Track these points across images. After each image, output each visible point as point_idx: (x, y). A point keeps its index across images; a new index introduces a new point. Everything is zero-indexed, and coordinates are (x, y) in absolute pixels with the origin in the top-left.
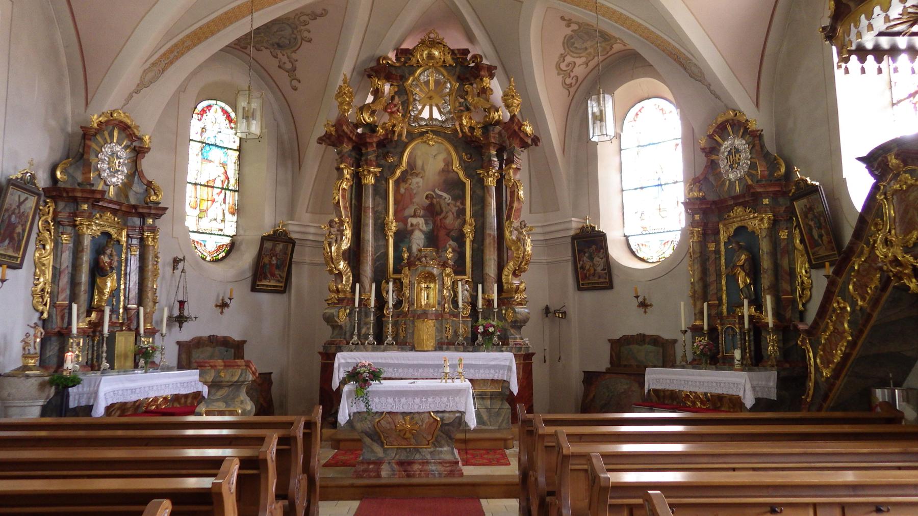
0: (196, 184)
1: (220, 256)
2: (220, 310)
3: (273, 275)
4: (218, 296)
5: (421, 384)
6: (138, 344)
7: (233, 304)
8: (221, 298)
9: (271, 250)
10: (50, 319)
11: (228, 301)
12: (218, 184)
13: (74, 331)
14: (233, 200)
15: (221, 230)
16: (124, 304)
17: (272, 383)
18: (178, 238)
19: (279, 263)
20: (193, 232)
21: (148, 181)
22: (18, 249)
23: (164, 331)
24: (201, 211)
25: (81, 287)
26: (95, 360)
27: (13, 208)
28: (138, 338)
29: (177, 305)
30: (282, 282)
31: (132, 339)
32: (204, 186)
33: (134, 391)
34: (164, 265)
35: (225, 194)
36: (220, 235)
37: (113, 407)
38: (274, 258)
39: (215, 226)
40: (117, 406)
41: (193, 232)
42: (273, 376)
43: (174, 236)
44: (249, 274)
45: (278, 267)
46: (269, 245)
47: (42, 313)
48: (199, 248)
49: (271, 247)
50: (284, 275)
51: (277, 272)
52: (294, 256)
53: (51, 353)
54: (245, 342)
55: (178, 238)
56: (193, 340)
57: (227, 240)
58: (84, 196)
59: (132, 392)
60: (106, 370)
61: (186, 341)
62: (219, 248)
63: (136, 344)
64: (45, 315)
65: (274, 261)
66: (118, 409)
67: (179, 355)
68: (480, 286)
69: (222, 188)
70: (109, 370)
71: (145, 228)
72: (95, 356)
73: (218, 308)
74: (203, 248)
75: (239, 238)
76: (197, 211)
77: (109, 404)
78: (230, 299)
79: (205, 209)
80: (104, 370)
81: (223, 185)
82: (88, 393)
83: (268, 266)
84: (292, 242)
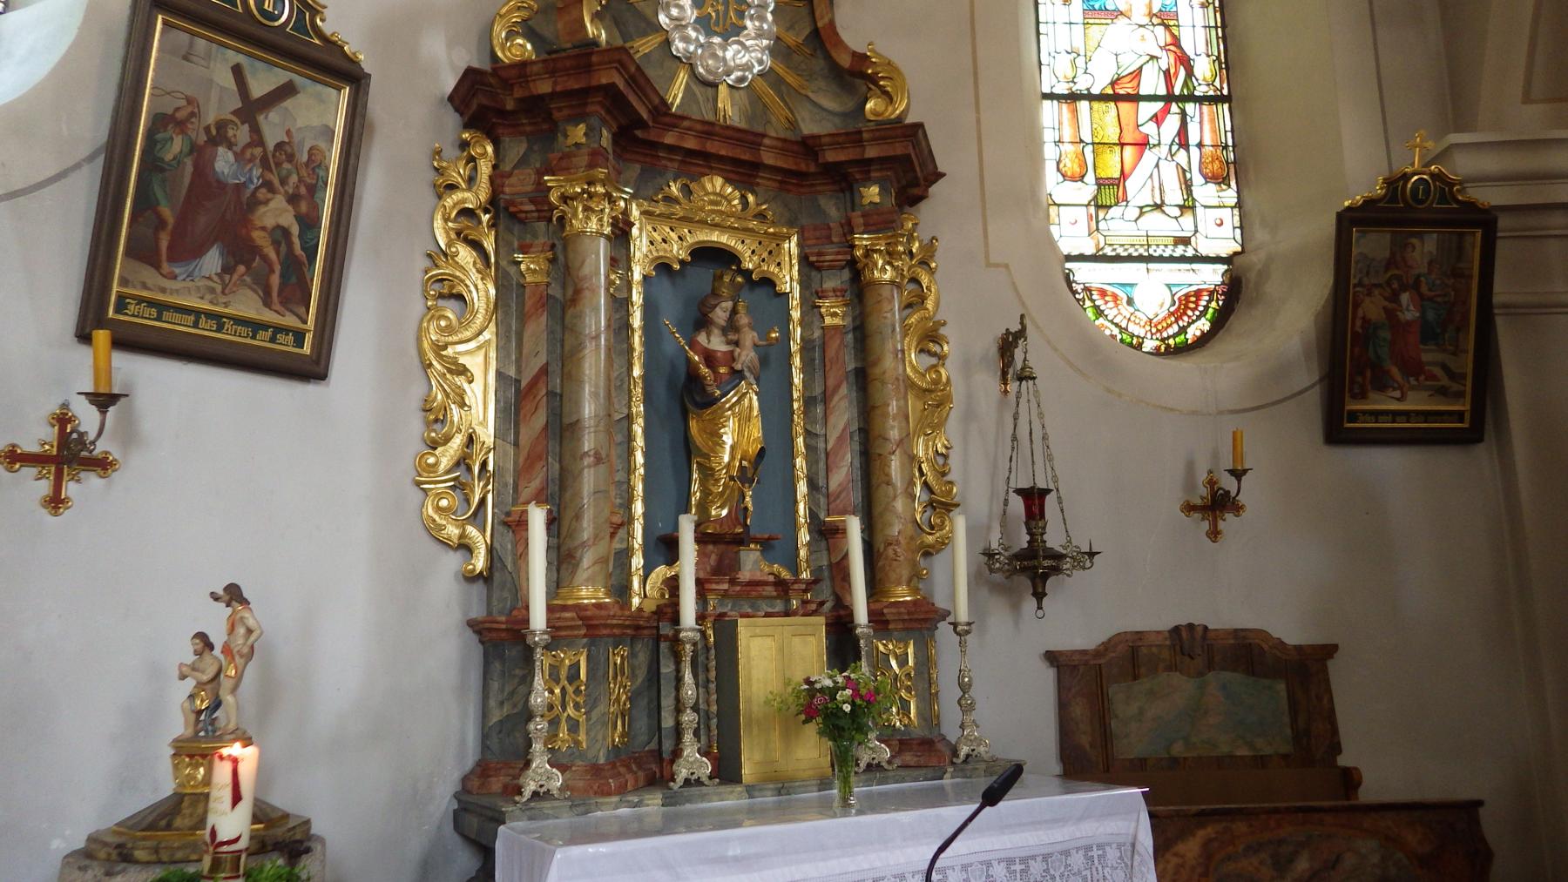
0: (1072, 98)
1: (1194, 332)
2: (1206, 525)
3: (1413, 369)
4: (1190, 467)
5: (637, 321)
7: (1250, 493)
8: (1202, 476)
9: (1390, 263)
10: (497, 575)
11: (1229, 483)
12: (1152, 83)
13: (538, 619)
14: (1214, 131)
15: (1185, 241)
16: (813, 515)
17: (1488, 855)
18: (1006, 266)
19: (1431, 315)
20: (1081, 258)
21: (854, 54)
22: (297, 293)
23: (963, 614)
24: (1101, 183)
25: (579, 440)
27: (211, 117)
29: (1017, 504)
30: (1459, 395)
32: (1102, 98)
33: (1095, 853)
34: (966, 367)
35: (1183, 114)
36: (1182, 259)
38: (1405, 298)
39: (1162, 226)
41: (1081, 258)
42: (1483, 812)
43: (993, 260)
44: (1307, 376)
45: (1429, 334)
46: (1372, 245)
48: (1111, 313)
49: (1387, 254)
50: (1467, 364)
51: (1429, 356)
52: (1499, 286)
54: (1329, 650)
55: (1006, 266)
56: (1107, 646)
57: (1212, 276)
58: (558, 88)
60: (699, 782)
61: (1084, 652)
62: (1185, 304)
64: (480, 562)
65: (1409, 310)
67: (1063, 706)
69: (1169, 98)
71: (858, 220)
73: (1197, 516)
74: (1126, 310)
75: (1254, 258)
76: (1087, 191)
78: (1238, 474)
79: (1117, 175)
81: (1169, 83)
83: (1385, 334)
84: (1484, 220)
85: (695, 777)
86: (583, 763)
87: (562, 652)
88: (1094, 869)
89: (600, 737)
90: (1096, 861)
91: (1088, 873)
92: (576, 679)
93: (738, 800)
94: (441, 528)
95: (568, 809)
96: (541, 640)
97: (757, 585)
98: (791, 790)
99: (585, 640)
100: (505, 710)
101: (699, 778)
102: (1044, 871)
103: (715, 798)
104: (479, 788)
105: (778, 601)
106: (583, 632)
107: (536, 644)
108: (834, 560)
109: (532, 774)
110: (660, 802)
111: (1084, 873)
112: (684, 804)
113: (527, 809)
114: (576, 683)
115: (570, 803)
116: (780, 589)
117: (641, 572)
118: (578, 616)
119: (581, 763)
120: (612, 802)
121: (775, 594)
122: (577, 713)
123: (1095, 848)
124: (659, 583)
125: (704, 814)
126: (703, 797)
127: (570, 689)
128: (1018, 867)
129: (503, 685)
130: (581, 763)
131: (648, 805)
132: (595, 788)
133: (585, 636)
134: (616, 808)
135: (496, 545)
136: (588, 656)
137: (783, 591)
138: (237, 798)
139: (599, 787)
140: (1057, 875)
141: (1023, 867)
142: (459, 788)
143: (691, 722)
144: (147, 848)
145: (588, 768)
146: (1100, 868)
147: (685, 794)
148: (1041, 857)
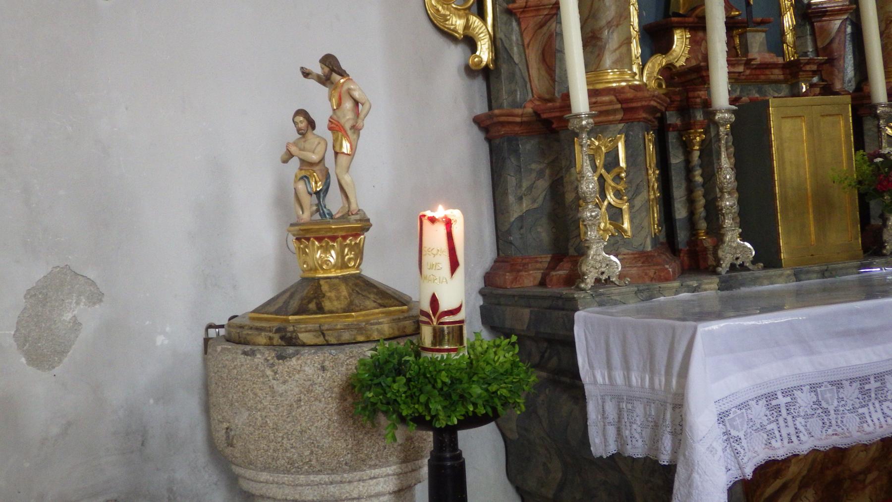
6: (870, 148)
10: (504, 68)
13: (581, 103)
26: (703, 225)
28: (869, 125)
31: (843, 127)
33: (873, 385)
37: (777, 474)
40: (793, 469)
47: (470, 43)
53: (526, 205)
59: (865, 393)
60: (743, 267)
63: (859, 144)
64: (484, 53)
66: (804, 484)
68: (653, 236)
70: (758, 271)
72: (701, 211)
77: (749, 472)
80: (733, 267)
82: (649, 402)
85: (739, 262)
86: (630, 252)
87: (596, 139)
88: (781, 420)
89: (645, 224)
90: (784, 412)
91: (773, 426)
92: (615, 167)
93: (786, 283)
94: (445, 18)
95: (634, 295)
96: (588, 123)
97: (766, 68)
98: (834, 273)
99: (621, 126)
100: (524, 205)
101: (743, 262)
102: (814, 403)
103: (765, 281)
104: (512, 283)
105: (784, 85)
106: (619, 116)
107: (582, 128)
108: (820, 45)
109: (592, 262)
110: (717, 287)
111: (769, 427)
112: (739, 288)
113: (597, 296)
114: (616, 170)
115: (636, 289)
116: (788, 71)
117: (640, 61)
118: (618, 100)
119: (626, 251)
120: (673, 288)
121: (781, 77)
122: (618, 201)
123: (780, 395)
124: (655, 74)
125: (758, 297)
126: (755, 281)
127: (609, 178)
128: (782, 400)
129: (521, 181)
130: (626, 251)
131: (705, 290)
132: (651, 273)
133: (621, 121)
134: (677, 293)
135: (500, 35)
136: (626, 141)
137: (791, 74)
138: (454, 265)
139: (655, 273)
140: (831, 409)
141: (878, 384)
142: (482, 285)
143: (732, 207)
144: (310, 331)
145: (636, 256)
146: (789, 418)
147: (740, 278)
148: (808, 387)
